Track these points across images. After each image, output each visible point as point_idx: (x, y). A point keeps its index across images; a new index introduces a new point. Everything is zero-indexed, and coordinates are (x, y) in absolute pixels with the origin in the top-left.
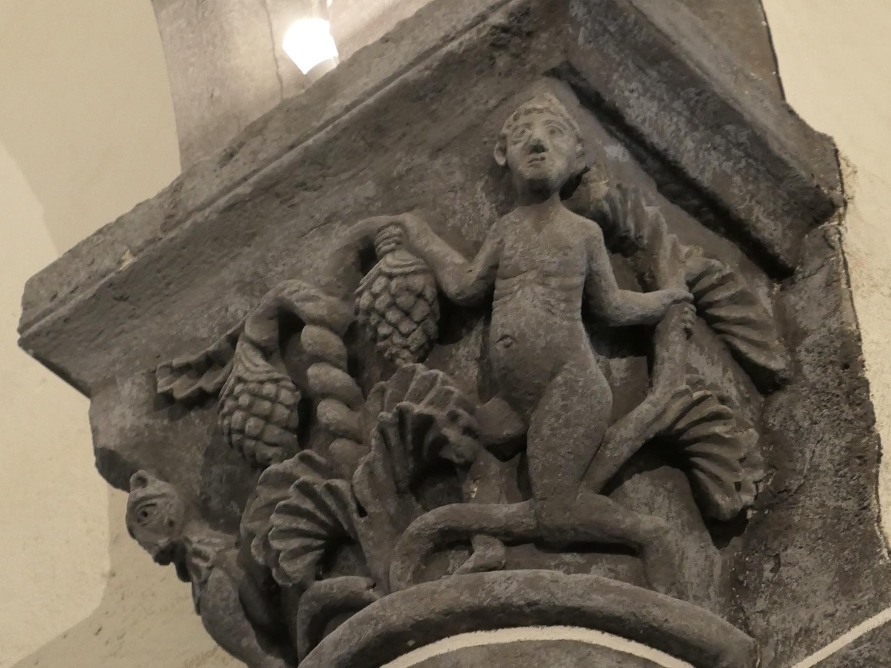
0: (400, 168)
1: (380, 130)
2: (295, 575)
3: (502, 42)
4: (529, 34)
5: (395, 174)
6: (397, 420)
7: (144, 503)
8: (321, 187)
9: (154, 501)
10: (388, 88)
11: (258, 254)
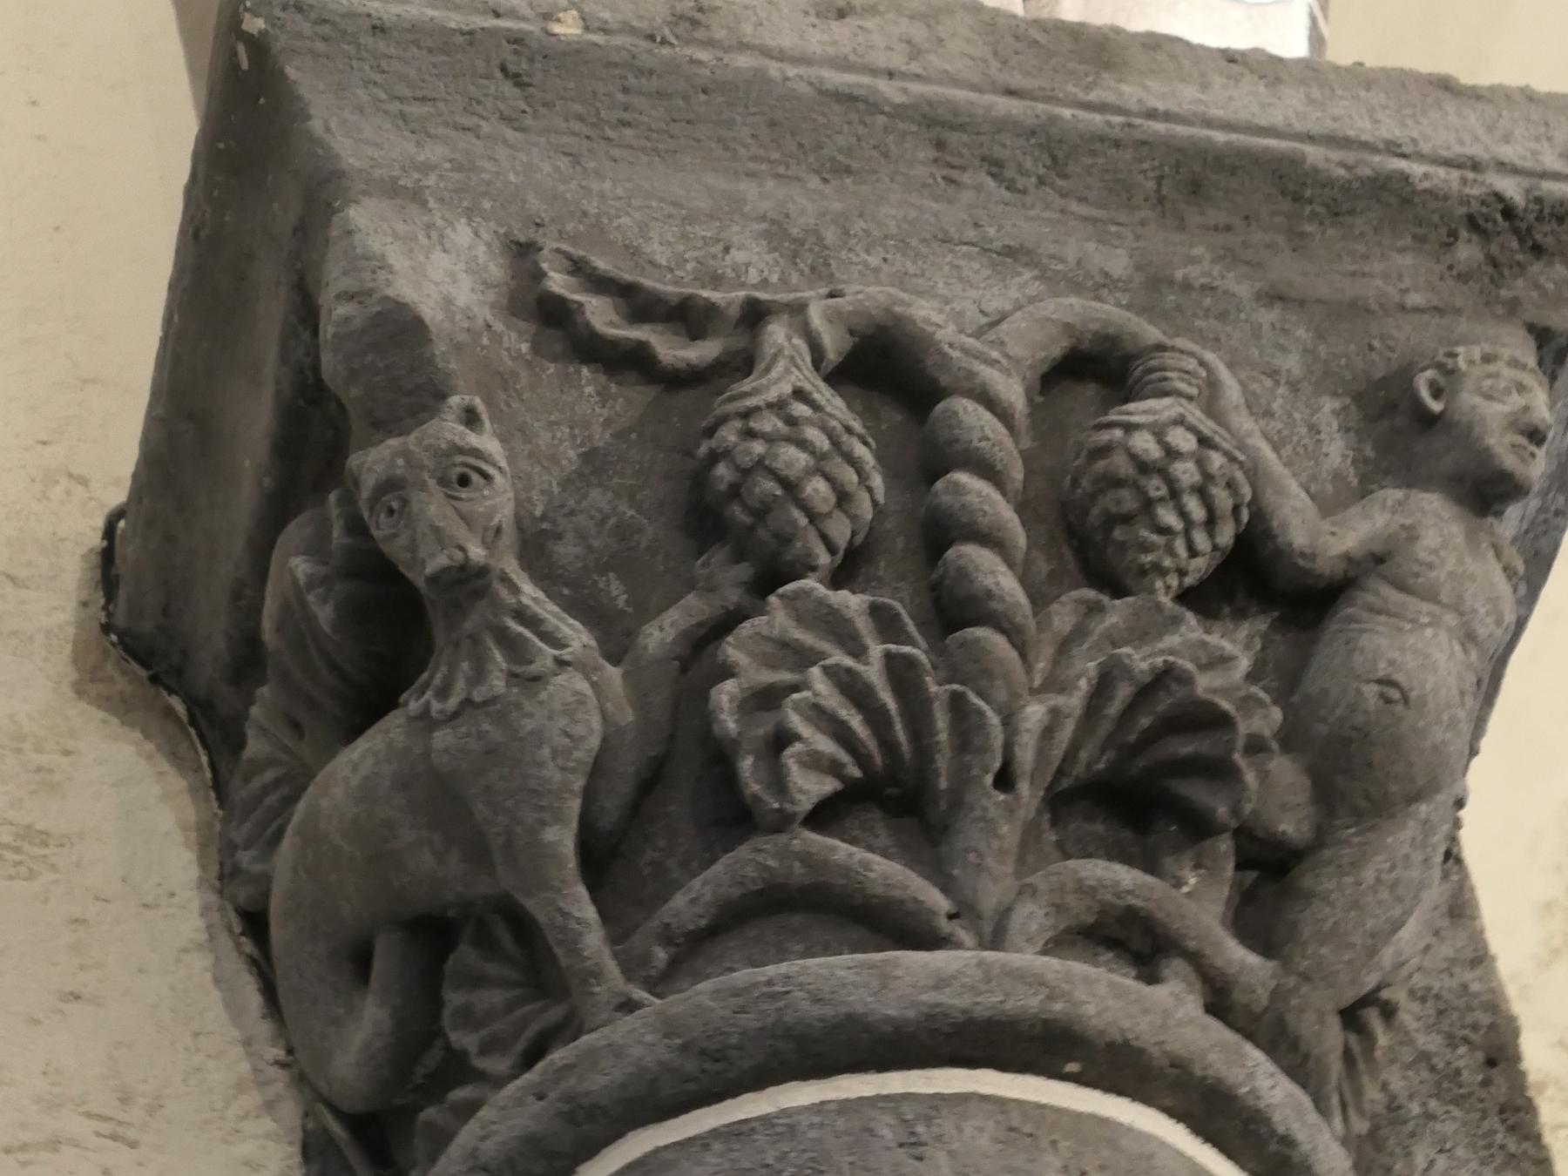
0: (1193, 272)
1: (1196, 190)
2: (798, 796)
3: (1490, 225)
4: (1537, 250)
5: (1179, 274)
6: (1148, 679)
7: (471, 461)
8: (1024, 192)
9: (491, 471)
10: (1272, 143)
11: (837, 206)
